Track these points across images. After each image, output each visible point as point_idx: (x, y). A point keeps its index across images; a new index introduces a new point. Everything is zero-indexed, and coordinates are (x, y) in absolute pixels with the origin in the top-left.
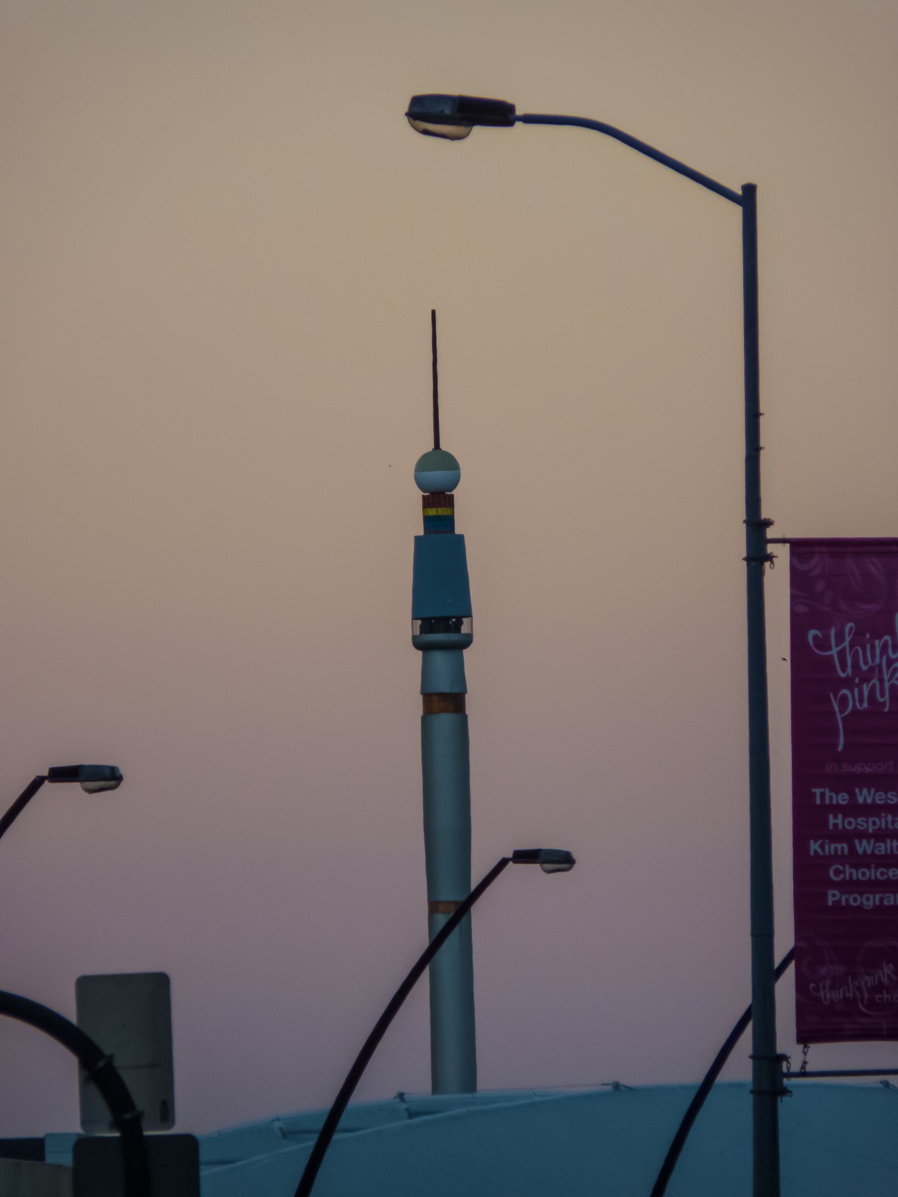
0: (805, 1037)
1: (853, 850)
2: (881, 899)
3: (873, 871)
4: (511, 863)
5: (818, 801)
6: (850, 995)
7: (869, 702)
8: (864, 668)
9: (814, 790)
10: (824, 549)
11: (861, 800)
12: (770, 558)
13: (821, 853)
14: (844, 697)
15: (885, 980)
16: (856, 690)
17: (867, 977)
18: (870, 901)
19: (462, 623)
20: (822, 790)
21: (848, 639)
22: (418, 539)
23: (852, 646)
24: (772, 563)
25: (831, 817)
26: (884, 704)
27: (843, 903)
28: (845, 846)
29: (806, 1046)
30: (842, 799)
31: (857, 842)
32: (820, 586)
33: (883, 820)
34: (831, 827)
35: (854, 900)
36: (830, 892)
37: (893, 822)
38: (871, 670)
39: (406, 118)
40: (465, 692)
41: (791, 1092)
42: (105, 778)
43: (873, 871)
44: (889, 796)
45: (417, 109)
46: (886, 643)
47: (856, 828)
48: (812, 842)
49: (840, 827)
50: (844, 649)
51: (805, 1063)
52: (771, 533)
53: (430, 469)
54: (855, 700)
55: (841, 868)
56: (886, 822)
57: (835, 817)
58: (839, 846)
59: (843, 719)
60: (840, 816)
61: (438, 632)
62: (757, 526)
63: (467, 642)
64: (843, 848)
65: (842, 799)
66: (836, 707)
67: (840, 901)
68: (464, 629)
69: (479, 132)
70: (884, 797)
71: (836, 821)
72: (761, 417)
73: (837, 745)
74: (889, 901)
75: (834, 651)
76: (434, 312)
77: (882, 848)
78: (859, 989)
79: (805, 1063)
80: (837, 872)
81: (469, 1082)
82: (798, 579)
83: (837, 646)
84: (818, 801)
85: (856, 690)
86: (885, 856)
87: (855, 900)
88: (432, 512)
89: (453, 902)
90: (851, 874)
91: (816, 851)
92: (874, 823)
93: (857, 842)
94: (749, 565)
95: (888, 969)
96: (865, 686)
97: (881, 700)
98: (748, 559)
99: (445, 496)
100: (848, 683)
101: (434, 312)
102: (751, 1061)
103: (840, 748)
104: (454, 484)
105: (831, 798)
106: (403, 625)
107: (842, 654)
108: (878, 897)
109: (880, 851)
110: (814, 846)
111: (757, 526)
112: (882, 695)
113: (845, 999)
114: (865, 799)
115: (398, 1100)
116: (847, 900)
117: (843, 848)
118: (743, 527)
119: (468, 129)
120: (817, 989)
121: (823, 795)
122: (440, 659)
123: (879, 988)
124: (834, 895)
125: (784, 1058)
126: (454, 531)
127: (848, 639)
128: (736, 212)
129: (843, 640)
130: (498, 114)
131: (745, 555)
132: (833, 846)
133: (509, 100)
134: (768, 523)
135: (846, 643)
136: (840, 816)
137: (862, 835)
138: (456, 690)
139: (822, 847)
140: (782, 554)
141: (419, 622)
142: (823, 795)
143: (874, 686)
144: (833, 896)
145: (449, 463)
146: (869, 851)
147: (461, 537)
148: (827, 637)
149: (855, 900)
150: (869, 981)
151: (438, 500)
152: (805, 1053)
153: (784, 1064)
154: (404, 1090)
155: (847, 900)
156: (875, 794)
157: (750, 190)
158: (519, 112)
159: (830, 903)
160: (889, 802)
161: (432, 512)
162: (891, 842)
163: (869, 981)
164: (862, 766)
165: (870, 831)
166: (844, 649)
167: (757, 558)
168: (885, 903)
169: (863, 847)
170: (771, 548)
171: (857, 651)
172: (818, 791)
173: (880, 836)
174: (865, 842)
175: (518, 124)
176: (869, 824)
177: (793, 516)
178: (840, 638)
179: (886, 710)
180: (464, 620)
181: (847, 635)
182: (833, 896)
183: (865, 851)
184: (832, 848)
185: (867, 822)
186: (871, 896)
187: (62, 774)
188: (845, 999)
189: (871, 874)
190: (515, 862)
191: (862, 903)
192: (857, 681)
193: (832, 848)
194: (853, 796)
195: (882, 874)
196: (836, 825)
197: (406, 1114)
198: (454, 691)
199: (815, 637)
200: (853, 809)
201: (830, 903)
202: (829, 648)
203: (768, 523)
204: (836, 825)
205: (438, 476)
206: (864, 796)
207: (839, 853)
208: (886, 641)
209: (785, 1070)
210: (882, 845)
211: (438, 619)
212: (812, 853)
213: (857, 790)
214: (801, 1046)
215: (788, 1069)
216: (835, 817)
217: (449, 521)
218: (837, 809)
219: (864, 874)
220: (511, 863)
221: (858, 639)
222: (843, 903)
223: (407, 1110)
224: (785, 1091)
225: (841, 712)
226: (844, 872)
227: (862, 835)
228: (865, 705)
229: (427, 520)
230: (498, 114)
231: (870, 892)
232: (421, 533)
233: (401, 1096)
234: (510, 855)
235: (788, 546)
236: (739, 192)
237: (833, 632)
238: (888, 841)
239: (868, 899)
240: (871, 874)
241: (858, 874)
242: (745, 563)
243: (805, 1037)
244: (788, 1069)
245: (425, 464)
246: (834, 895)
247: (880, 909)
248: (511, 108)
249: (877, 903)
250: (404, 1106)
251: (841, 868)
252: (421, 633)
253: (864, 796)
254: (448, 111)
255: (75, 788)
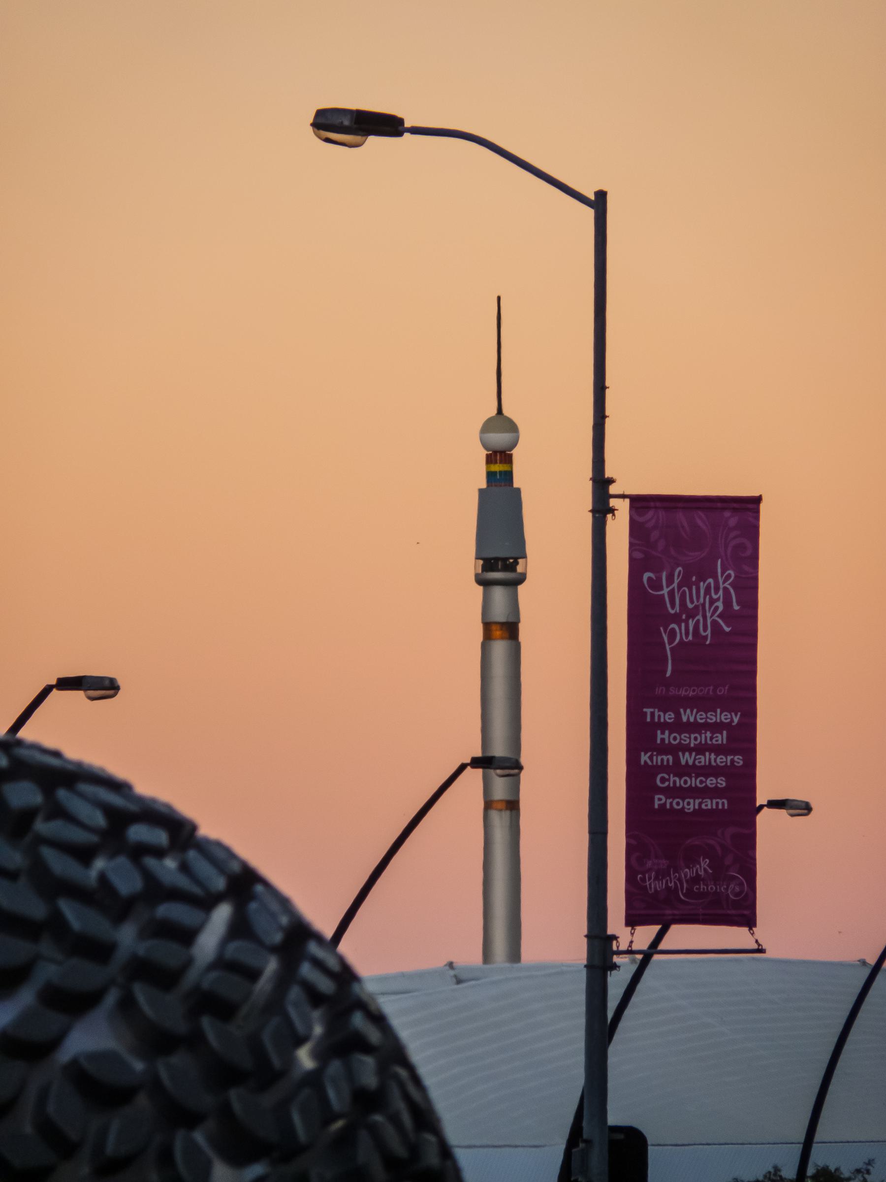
0: (632, 921)
1: (677, 760)
2: (700, 804)
3: (693, 779)
4: (469, 768)
5: (648, 720)
6: (672, 885)
7: (693, 636)
8: (690, 606)
9: (645, 710)
10: (658, 504)
11: (685, 719)
12: (612, 511)
13: (650, 763)
14: (673, 630)
15: (702, 873)
16: (683, 625)
17: (687, 870)
18: (691, 805)
19: (518, 563)
20: (652, 710)
21: (676, 581)
22: (481, 491)
23: (679, 587)
24: (614, 515)
25: (659, 732)
26: (706, 637)
27: (668, 806)
28: (671, 758)
29: (750, 929)
30: (669, 717)
31: (680, 754)
32: (655, 535)
33: (703, 736)
34: (659, 741)
35: (677, 804)
36: (657, 797)
37: (711, 739)
38: (696, 607)
39: (311, 128)
40: (519, 622)
41: (619, 967)
42: (103, 687)
43: (693, 779)
44: (709, 715)
45: (321, 120)
46: (709, 585)
47: (680, 743)
48: (643, 754)
49: (667, 742)
50: (673, 589)
51: (631, 942)
52: (613, 489)
53: (494, 431)
54: (682, 633)
55: (704, 779)
56: (706, 738)
57: (663, 733)
58: (665, 758)
59: (671, 649)
60: (667, 732)
61: (498, 570)
62: (601, 484)
63: (522, 579)
64: (668, 760)
65: (669, 717)
66: (666, 641)
67: (665, 804)
68: (520, 569)
69: (373, 141)
70: (704, 716)
71: (663, 736)
72: (607, 390)
73: (665, 671)
74: (706, 805)
75: (665, 591)
76: (499, 298)
77: (703, 760)
78: (680, 880)
79: (631, 942)
80: (663, 780)
81: (515, 955)
82: (636, 530)
83: (667, 587)
84: (648, 720)
85: (683, 625)
86: (704, 767)
87: (678, 804)
88: (497, 468)
89: (501, 801)
90: (675, 782)
91: (645, 762)
92: (696, 739)
93: (680, 754)
94: (594, 517)
95: (705, 863)
96: (690, 621)
97: (704, 634)
98: (593, 511)
99: (506, 455)
100: (676, 618)
101: (499, 298)
102: (585, 940)
103: (668, 674)
104: (514, 445)
105: (659, 717)
106: (468, 564)
107: (671, 594)
108: (697, 801)
109: (700, 762)
110: (644, 758)
111: (601, 484)
112: (705, 630)
113: (668, 888)
114: (688, 718)
115: (447, 968)
116: (671, 803)
117: (668, 760)
118: (590, 484)
119: (364, 138)
120: (643, 880)
121: (653, 714)
122: (499, 594)
123: (696, 879)
124: (660, 799)
125: (614, 937)
126: (512, 485)
127: (676, 581)
128: (589, 214)
129: (673, 582)
130: (389, 125)
131: (590, 508)
132: (659, 758)
133: (399, 114)
134: (611, 481)
135: (675, 585)
136: (667, 732)
137: (686, 749)
138: (511, 620)
139: (651, 758)
140: (622, 507)
141: (481, 562)
142: (653, 714)
143: (698, 621)
144: (659, 800)
145: (512, 427)
146: (690, 762)
147: (518, 491)
148: (660, 579)
149: (678, 804)
150: (688, 872)
151: (500, 458)
152: (632, 934)
153: (614, 943)
154: (454, 960)
155: (671, 803)
156: (697, 713)
157: (601, 196)
158: (407, 124)
159: (656, 806)
160: (709, 720)
161: (497, 468)
162: (710, 755)
163: (688, 872)
164: (686, 691)
165: (692, 745)
166: (673, 589)
167: (601, 509)
168: (703, 806)
169: (686, 758)
170: (613, 502)
171: (684, 592)
172: (648, 711)
173: (700, 749)
174: (687, 754)
175: (407, 135)
176: (692, 739)
177: (631, 476)
178: (670, 581)
179: (708, 642)
180: (520, 561)
181: (676, 577)
182: (659, 800)
183: (687, 761)
184: (658, 760)
185: (690, 738)
186: (692, 801)
187: (67, 684)
188: (668, 888)
189: (694, 782)
190: (473, 767)
191: (683, 808)
192: (684, 617)
193: (658, 760)
194: (678, 716)
195: (701, 782)
196: (663, 740)
197: (454, 980)
198: (510, 620)
199: (649, 579)
200: (678, 727)
201: (656, 806)
202: (661, 588)
203: (611, 481)
204: (663, 740)
205: (499, 439)
206: (687, 716)
207: (665, 763)
208: (710, 584)
209: (615, 948)
210: (703, 757)
211: (497, 559)
212: (642, 763)
213: (682, 711)
214: (630, 928)
215: (618, 947)
216: (663, 733)
217: (508, 476)
218: (664, 726)
219: (686, 782)
220: (469, 768)
221: (685, 582)
222: (668, 806)
223: (455, 976)
224: (615, 967)
225: (670, 643)
226: (669, 780)
227: (686, 749)
228: (690, 637)
229: (490, 475)
230: (389, 125)
231: (690, 798)
232: (484, 485)
233: (451, 965)
234: (468, 761)
235: (627, 501)
236: (592, 197)
237: (664, 575)
238: (707, 754)
239: (689, 804)
240: (694, 782)
241: (680, 782)
242: (590, 514)
243: (632, 921)
244: (618, 947)
245: (488, 427)
246: (660, 799)
247: (699, 812)
248: (401, 121)
249: (697, 807)
250: (452, 973)
251: (704, 779)
252: (483, 571)
253: (687, 716)
254: (346, 123)
255: (78, 696)
